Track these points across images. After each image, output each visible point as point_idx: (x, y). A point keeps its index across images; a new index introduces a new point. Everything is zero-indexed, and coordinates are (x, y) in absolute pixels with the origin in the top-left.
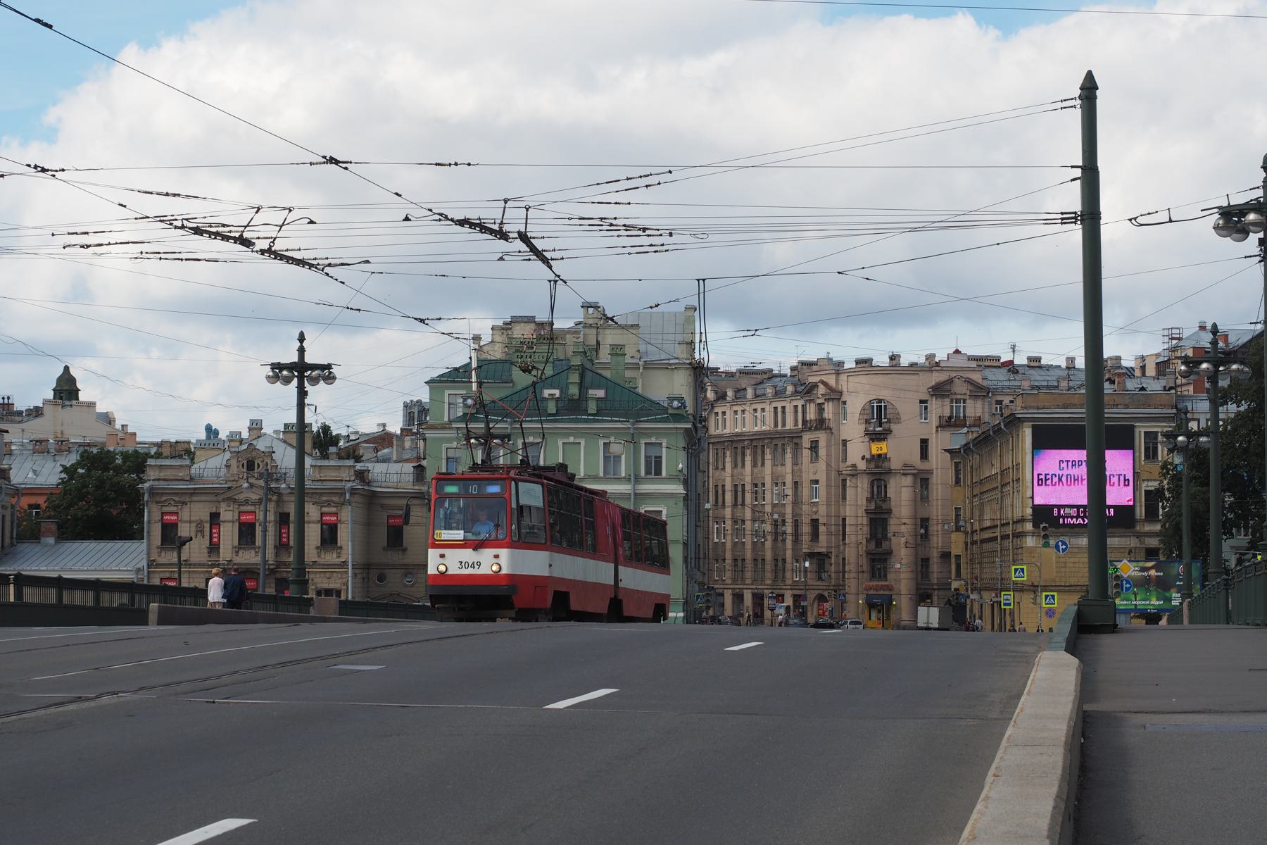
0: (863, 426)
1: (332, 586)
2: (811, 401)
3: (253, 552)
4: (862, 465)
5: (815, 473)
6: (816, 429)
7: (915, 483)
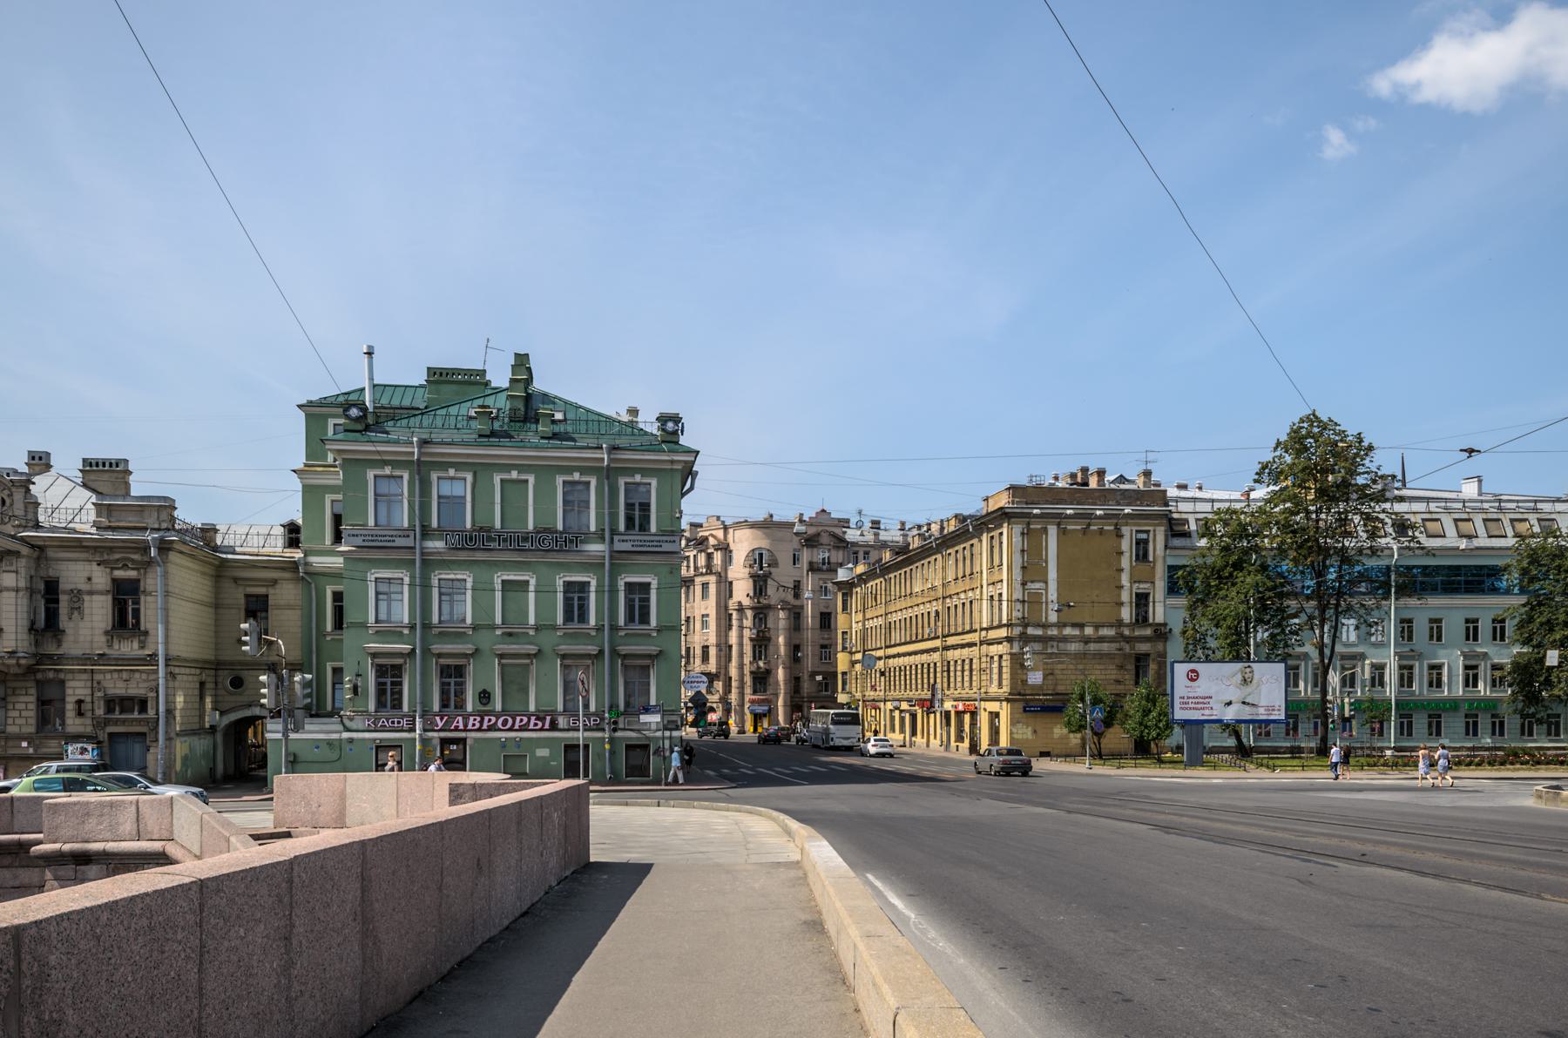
1: (133, 692)
2: (701, 551)
5: (706, 608)
7: (790, 615)
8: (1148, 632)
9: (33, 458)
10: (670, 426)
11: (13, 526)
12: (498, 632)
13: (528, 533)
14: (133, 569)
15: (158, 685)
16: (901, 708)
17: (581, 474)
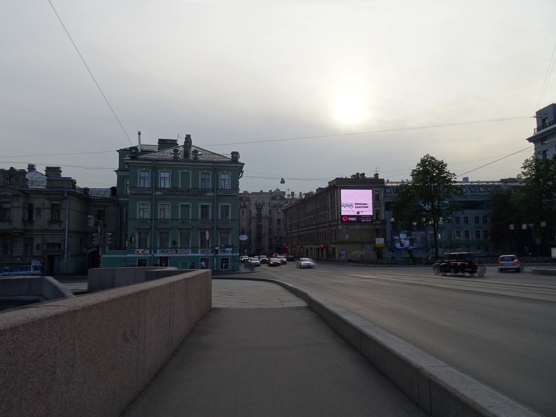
0: (255, 207)
1: (56, 241)
3: (8, 224)
4: (255, 216)
6: (244, 208)
8: (380, 222)
9: (30, 167)
10: (235, 155)
11: (19, 187)
12: (180, 221)
13: (189, 189)
14: (58, 201)
15: (65, 239)
16: (303, 247)
17: (207, 171)
